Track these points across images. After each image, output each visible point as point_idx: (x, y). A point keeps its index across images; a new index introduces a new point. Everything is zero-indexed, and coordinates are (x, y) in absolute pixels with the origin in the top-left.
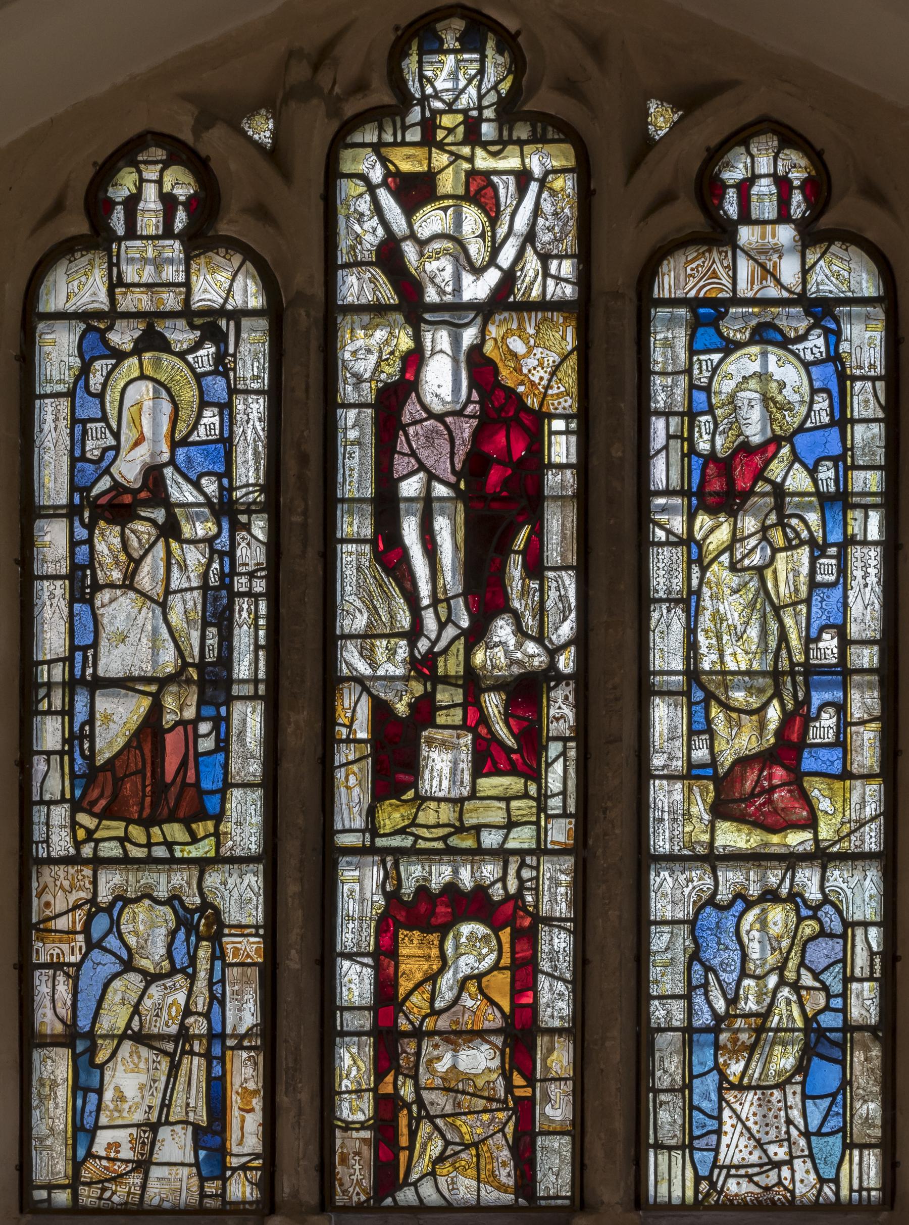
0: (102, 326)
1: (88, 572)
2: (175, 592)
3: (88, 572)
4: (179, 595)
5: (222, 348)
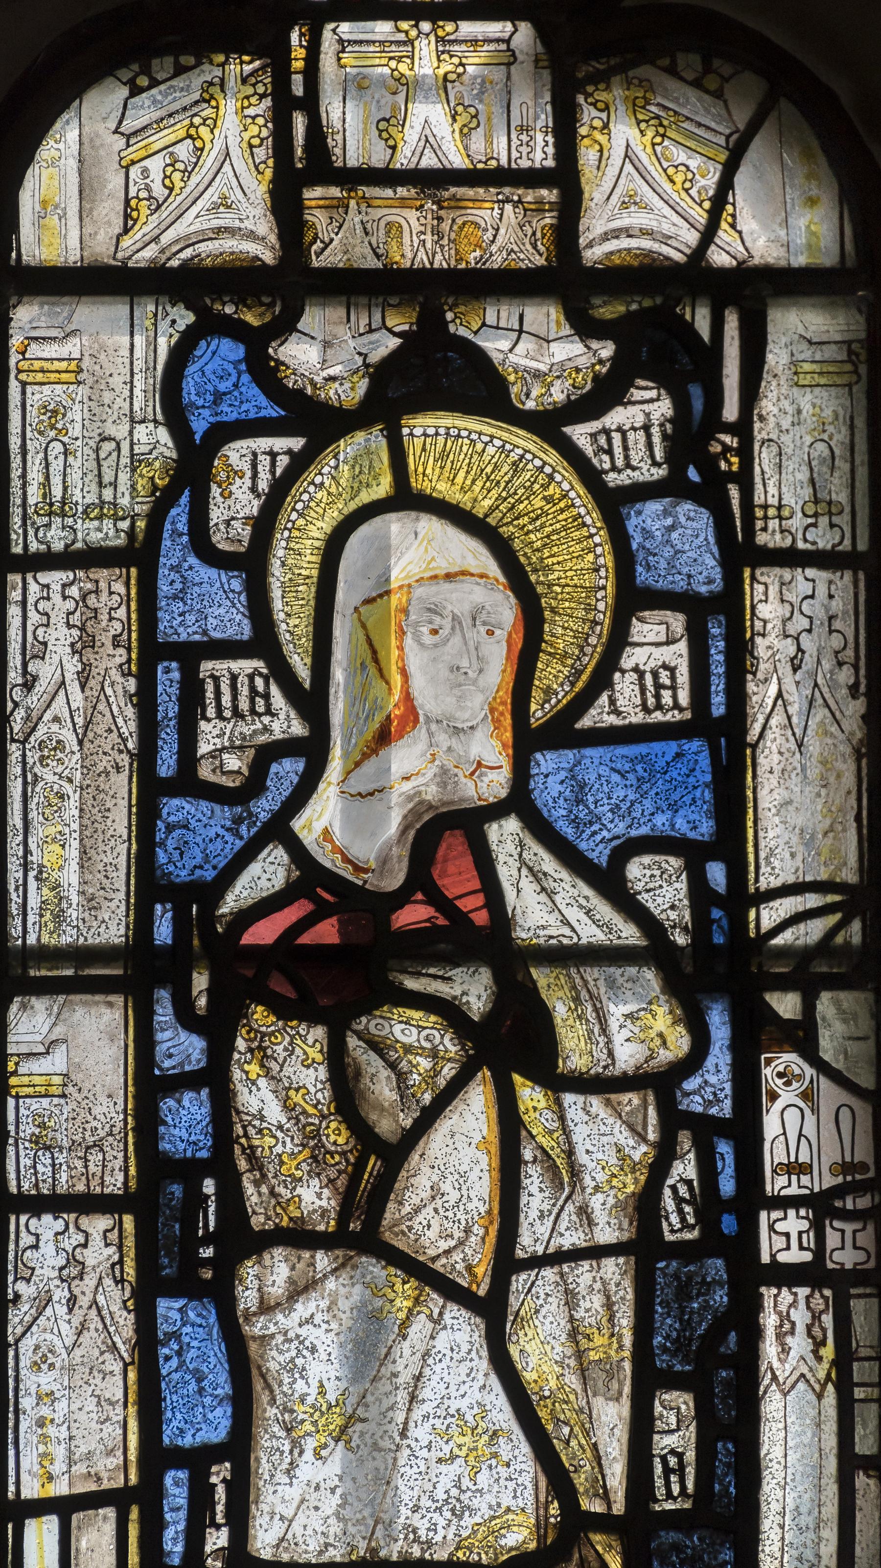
0: (251, 318)
1: (209, 1186)
2: (537, 1262)
3: (209, 1186)
4: (549, 1273)
5: (698, 405)
